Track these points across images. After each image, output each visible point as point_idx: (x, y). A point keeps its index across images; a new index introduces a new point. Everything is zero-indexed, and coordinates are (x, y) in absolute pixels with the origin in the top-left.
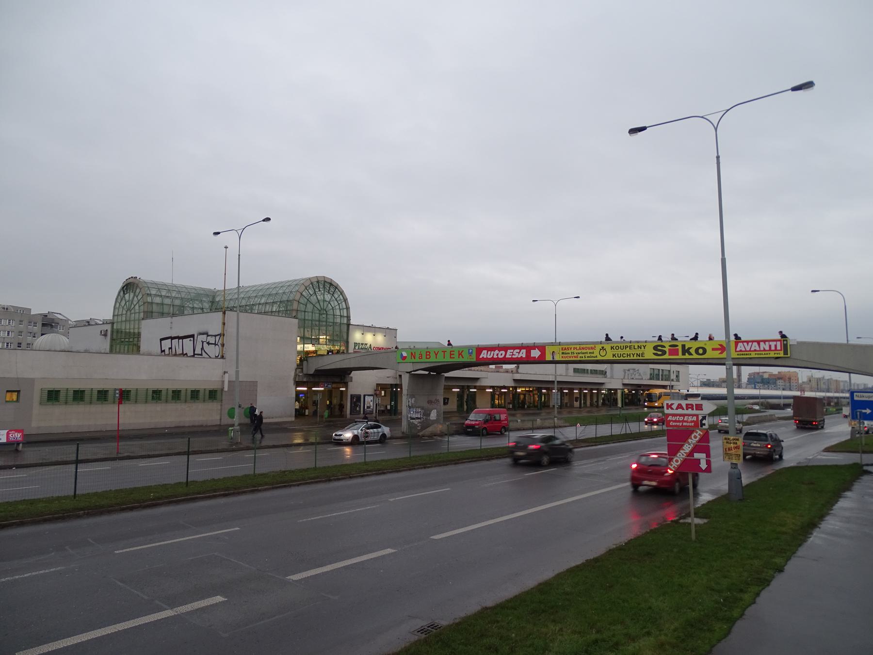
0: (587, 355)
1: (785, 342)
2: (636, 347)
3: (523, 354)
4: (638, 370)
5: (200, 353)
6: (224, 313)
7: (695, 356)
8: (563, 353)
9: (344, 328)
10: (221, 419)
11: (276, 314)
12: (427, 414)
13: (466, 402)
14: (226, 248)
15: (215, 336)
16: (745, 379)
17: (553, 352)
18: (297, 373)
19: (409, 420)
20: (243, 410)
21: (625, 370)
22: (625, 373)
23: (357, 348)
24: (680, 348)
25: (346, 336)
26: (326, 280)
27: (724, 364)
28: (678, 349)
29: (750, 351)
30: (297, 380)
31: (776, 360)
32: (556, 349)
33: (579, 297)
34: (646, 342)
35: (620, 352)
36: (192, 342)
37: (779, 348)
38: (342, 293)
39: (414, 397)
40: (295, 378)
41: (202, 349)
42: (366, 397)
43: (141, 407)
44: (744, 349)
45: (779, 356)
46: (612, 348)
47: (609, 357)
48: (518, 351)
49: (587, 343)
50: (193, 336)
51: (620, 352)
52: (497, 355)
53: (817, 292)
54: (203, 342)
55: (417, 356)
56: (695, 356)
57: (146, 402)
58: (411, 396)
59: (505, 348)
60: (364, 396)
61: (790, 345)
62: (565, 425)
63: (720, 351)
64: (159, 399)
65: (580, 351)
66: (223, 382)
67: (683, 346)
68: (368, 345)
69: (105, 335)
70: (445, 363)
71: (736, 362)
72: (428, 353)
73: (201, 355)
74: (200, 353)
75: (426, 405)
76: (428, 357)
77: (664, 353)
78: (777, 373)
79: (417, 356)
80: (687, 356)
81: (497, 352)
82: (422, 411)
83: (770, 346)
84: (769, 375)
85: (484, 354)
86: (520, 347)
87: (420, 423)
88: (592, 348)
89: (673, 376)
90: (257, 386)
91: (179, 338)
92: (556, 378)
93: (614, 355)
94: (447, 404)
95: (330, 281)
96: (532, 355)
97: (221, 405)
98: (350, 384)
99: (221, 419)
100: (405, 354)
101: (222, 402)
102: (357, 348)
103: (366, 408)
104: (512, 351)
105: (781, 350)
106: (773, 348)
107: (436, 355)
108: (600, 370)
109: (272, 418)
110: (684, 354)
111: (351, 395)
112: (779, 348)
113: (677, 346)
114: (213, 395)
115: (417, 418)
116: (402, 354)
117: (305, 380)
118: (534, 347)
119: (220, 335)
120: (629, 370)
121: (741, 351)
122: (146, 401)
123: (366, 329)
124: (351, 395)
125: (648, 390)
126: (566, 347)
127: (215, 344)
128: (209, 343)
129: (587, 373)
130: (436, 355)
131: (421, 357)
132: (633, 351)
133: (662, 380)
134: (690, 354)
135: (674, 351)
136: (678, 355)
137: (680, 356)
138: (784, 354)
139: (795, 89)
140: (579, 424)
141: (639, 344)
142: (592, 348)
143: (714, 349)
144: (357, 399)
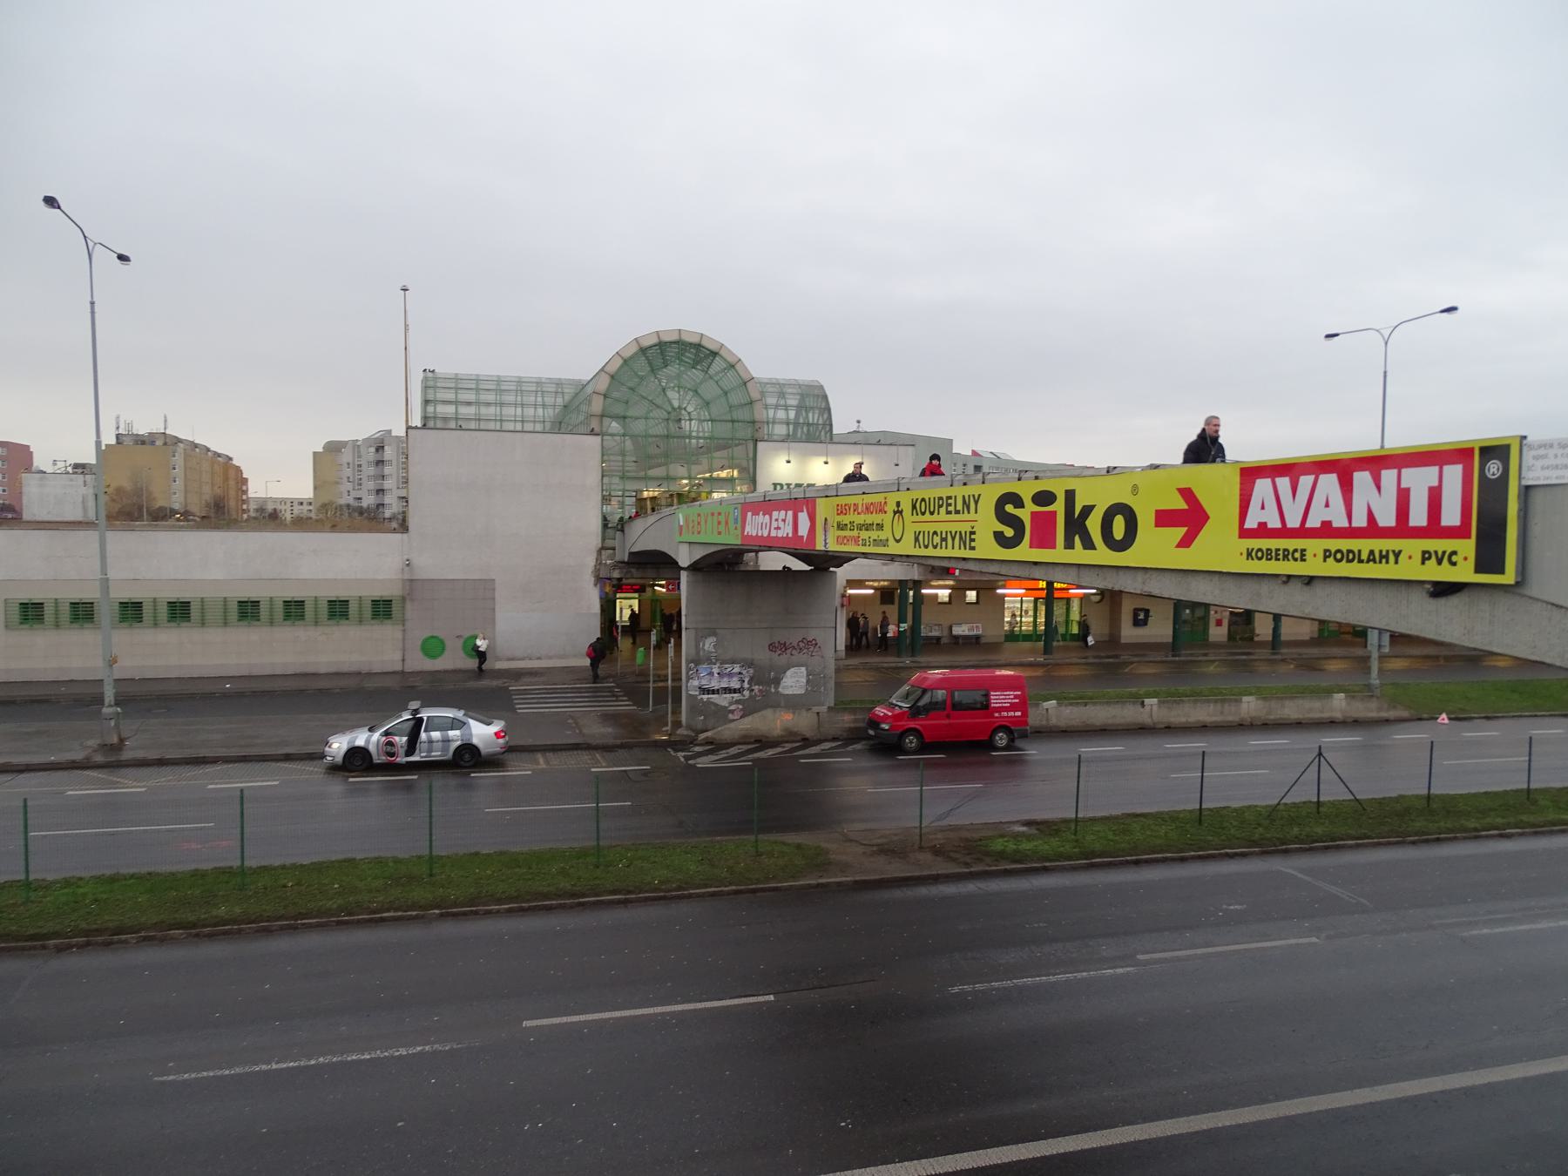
1: (1494, 468)
8: (841, 527)
10: (403, 660)
14: (859, 422)
18: (603, 557)
19: (694, 697)
20: (462, 640)
21: (1303, 560)
28: (1054, 513)
29: (1303, 532)
31: (1442, 601)
37: (1451, 516)
39: (715, 634)
43: (214, 635)
44: (1275, 523)
45: (1446, 574)
57: (226, 624)
61: (1527, 491)
62: (1384, 715)
63: (1180, 532)
64: (302, 617)
70: (729, 547)
82: (748, 673)
83: (1403, 497)
94: (1146, 624)
97: (404, 631)
99: (403, 660)
101: (404, 625)
105: (1460, 532)
106: (1418, 517)
109: (539, 658)
112: (1451, 516)
114: (382, 609)
115: (725, 689)
121: (1263, 531)
122: (156, 624)
138: (1480, 568)
140: (1444, 716)
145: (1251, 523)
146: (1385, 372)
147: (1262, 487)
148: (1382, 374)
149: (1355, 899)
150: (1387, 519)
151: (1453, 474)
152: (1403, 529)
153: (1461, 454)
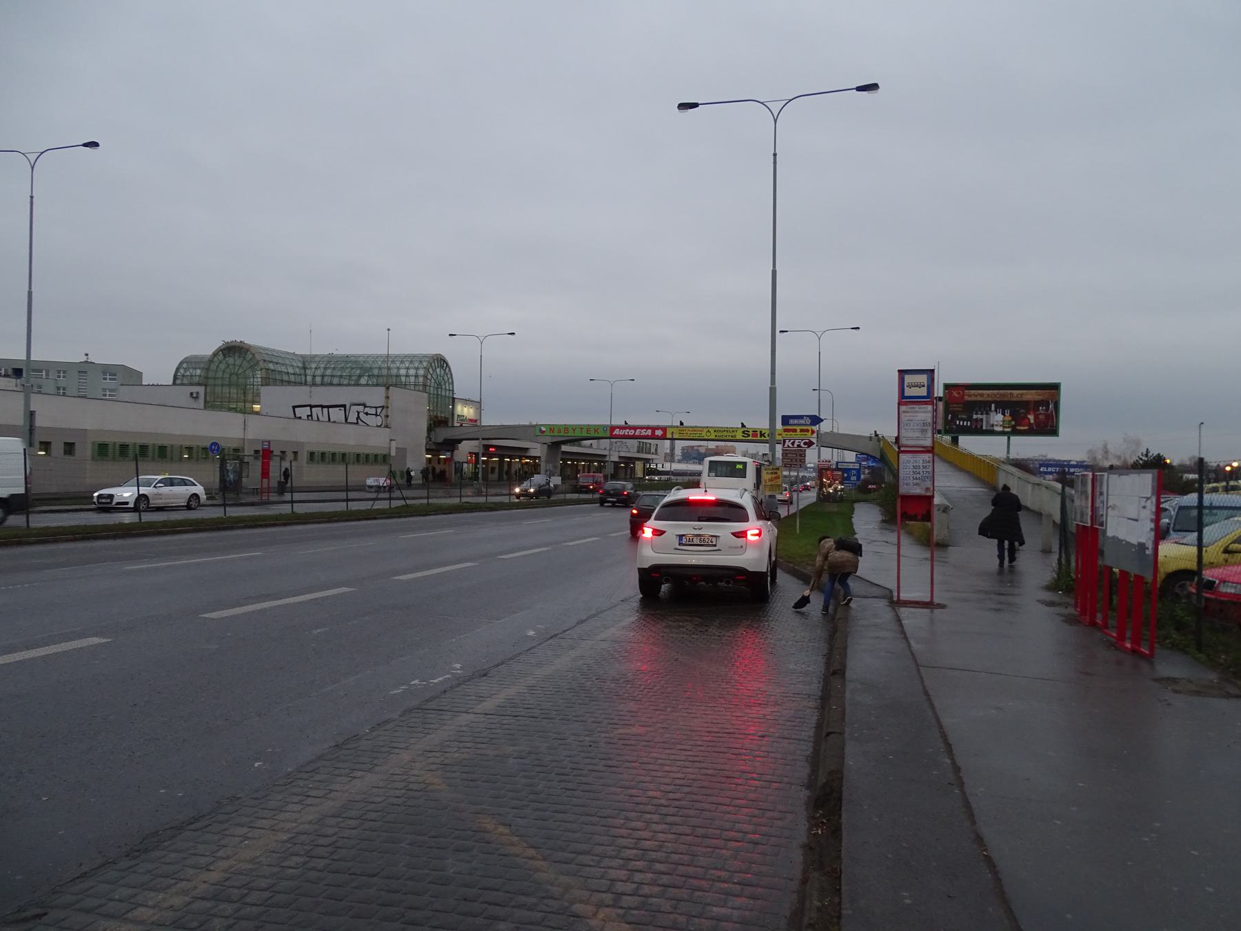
3: (649, 432)
6: (388, 388)
9: (451, 400)
11: (403, 386)
13: (429, 472)
14: (389, 330)
15: (376, 408)
16: (678, 452)
17: (672, 433)
24: (759, 433)
32: (672, 430)
33: (514, 334)
35: (720, 434)
40: (426, 446)
41: (358, 418)
46: (715, 431)
47: (713, 437)
50: (344, 406)
51: (720, 434)
54: (358, 413)
58: (547, 462)
59: (635, 428)
67: (761, 432)
69: (197, 398)
73: (357, 423)
74: (356, 422)
77: (749, 435)
78: (714, 447)
80: (763, 438)
81: (628, 430)
84: (706, 449)
85: (617, 432)
86: (647, 428)
88: (701, 431)
89: (653, 450)
90: (406, 452)
91: (322, 407)
93: (716, 436)
96: (656, 434)
100: (543, 429)
110: (761, 437)
113: (757, 431)
118: (658, 428)
119: (383, 407)
123: (467, 402)
127: (376, 415)
128: (367, 414)
131: (559, 431)
132: (730, 434)
133: (646, 453)
134: (765, 437)
136: (757, 437)
137: (759, 438)
139: (860, 89)
142: (701, 431)
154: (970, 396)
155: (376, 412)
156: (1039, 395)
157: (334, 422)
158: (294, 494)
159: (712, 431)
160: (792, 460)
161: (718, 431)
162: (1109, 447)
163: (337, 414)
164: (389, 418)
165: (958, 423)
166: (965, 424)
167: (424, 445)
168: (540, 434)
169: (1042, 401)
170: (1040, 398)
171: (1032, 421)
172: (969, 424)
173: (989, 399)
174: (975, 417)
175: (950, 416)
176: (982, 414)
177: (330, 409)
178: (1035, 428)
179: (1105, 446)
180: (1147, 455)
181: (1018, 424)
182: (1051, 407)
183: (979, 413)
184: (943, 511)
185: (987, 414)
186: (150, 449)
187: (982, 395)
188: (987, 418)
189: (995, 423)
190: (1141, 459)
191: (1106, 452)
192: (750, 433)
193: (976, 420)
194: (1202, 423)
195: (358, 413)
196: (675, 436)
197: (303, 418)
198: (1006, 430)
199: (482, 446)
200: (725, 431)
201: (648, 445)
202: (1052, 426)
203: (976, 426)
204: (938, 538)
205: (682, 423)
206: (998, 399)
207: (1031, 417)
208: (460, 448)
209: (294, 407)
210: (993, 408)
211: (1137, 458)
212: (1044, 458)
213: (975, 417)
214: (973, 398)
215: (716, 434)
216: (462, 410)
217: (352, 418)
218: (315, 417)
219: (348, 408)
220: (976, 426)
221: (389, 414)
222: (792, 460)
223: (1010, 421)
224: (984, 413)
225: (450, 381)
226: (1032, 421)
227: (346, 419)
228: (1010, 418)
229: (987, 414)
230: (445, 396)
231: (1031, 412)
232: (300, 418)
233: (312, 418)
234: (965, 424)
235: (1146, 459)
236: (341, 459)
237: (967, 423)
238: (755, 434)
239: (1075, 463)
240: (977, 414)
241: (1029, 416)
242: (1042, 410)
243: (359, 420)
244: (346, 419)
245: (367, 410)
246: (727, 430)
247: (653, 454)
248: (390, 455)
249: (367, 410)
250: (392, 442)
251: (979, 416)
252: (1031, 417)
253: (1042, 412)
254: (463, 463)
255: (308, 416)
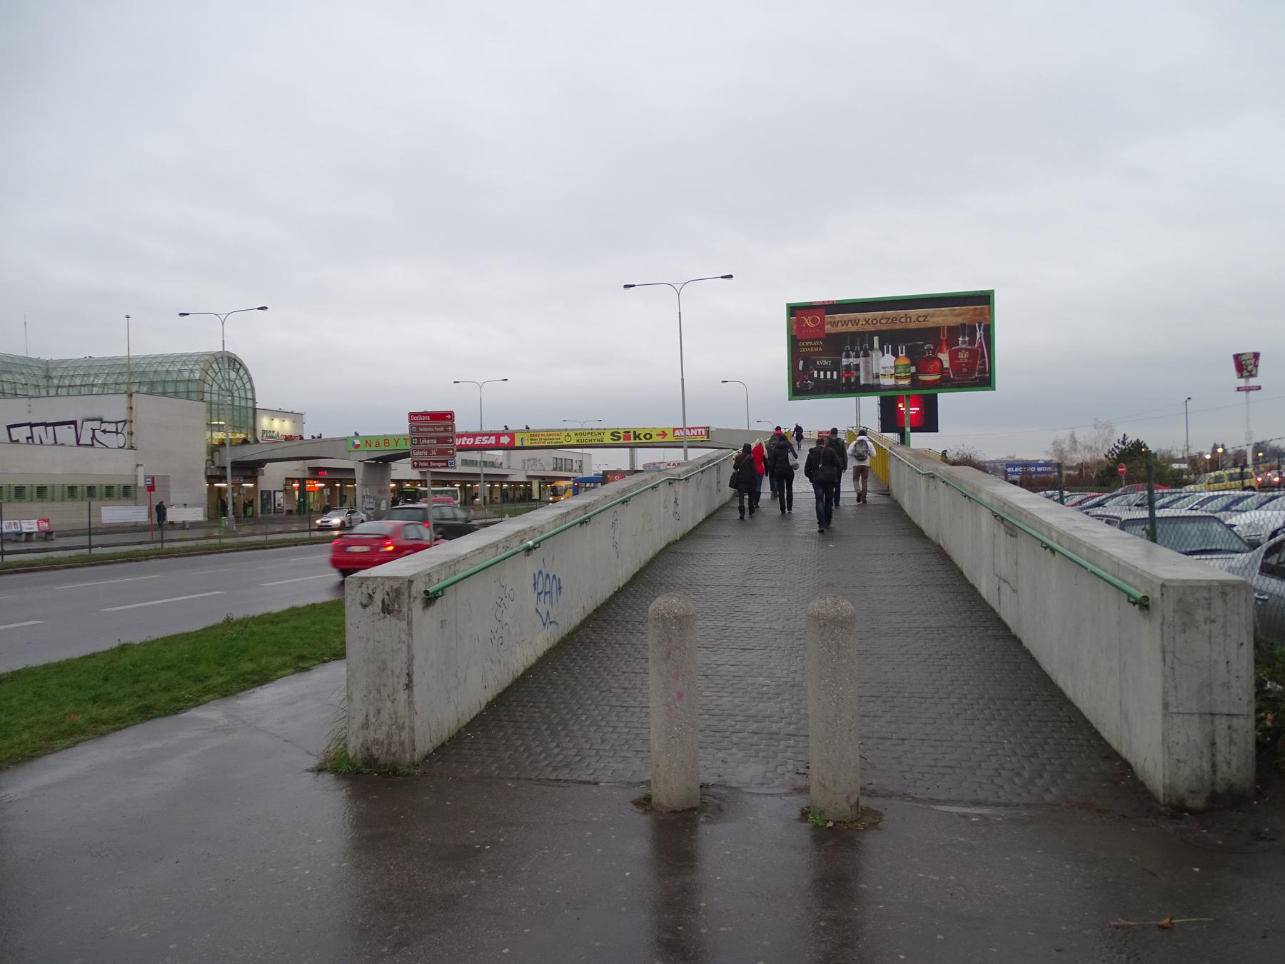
0: (553, 441)
2: (597, 433)
3: (493, 440)
4: (540, 460)
5: (80, 443)
6: (131, 396)
7: (644, 440)
8: (531, 440)
9: (250, 412)
12: (378, 505)
14: (128, 317)
15: (116, 423)
17: (522, 439)
21: (524, 460)
22: (525, 463)
23: (265, 436)
24: (632, 434)
25: (252, 422)
26: (231, 356)
27: (682, 447)
30: (209, 474)
32: (525, 436)
34: (605, 429)
35: (582, 438)
36: (73, 430)
37: (703, 433)
38: (246, 371)
40: (206, 472)
41: (93, 437)
42: (277, 493)
46: (576, 434)
47: (574, 442)
48: (488, 437)
49: (554, 430)
50: (74, 423)
51: (582, 438)
52: (466, 442)
53: (631, 288)
54: (94, 430)
55: (373, 444)
56: (644, 440)
57: (63, 500)
58: (365, 485)
59: (474, 436)
60: (275, 492)
65: (547, 437)
66: (136, 476)
67: (635, 432)
68: (276, 433)
71: (691, 444)
72: (387, 441)
73: (92, 445)
75: (376, 494)
76: (387, 444)
77: (619, 438)
79: (373, 444)
80: (638, 441)
81: (465, 439)
83: (698, 432)
86: (490, 435)
87: (373, 513)
89: (576, 467)
90: (169, 481)
91: (46, 425)
92: (482, 470)
93: (578, 441)
95: (234, 357)
96: (501, 442)
98: (260, 477)
102: (265, 436)
103: (276, 505)
104: (481, 438)
106: (700, 434)
107: (397, 442)
108: (490, 462)
110: (635, 439)
111: (262, 492)
112: (703, 433)
113: (629, 432)
116: (354, 443)
117: (218, 474)
119: (125, 421)
120: (529, 460)
121: (677, 436)
123: (275, 413)
124: (262, 492)
125: (551, 483)
126: (535, 434)
127: (117, 432)
128: (104, 431)
129: (476, 465)
130: (397, 442)
131: (378, 444)
132: (594, 437)
133: (565, 471)
134: (640, 439)
135: (627, 437)
136: (630, 440)
137: (632, 441)
141: (599, 431)
143: (658, 435)
144: (268, 496)
145: (676, 435)
146: (223, 341)
147: (677, 431)
148: (222, 343)
149: (567, 479)
150: (696, 434)
151: (703, 430)
152: (698, 435)
153: (704, 428)
154: (834, 324)
155: (117, 429)
156: (958, 315)
157: (63, 444)
158: (92, 537)
159: (572, 434)
160: (429, 451)
161: (581, 434)
162: (1077, 436)
163: (66, 434)
164: (133, 436)
165: (815, 376)
166: (829, 377)
167: (203, 471)
168: (352, 449)
169: (963, 325)
170: (959, 320)
171: (946, 365)
172: (835, 377)
173: (870, 328)
174: (845, 362)
175: (801, 362)
176: (857, 356)
177: (57, 428)
178: (952, 377)
179: (1073, 436)
180: (1124, 443)
181: (919, 372)
182: (978, 336)
183: (852, 354)
184: (386, 609)
185: (866, 355)
186: (79, 489)
187: (855, 322)
188: (867, 363)
189: (882, 372)
190: (1117, 447)
191: (1074, 441)
192: (621, 435)
193: (848, 366)
194: (1189, 398)
195: (94, 430)
196: (526, 444)
197: (21, 441)
198: (901, 382)
199: (307, 469)
200: (588, 434)
201: (569, 462)
202: (982, 371)
203: (848, 379)
204: (371, 735)
205: (528, 428)
206: (884, 328)
207: (944, 357)
208: (265, 472)
209: (9, 427)
210: (876, 345)
211: (1113, 446)
212: (1012, 459)
213: (845, 362)
214: (840, 329)
215: (579, 438)
216: (271, 424)
217: (86, 439)
218: (37, 440)
219: (79, 424)
220: (848, 379)
221: (133, 430)
222: (429, 451)
223: (907, 366)
224: (862, 353)
225: (248, 386)
226: (946, 365)
227: (78, 441)
228: (907, 362)
229: (866, 355)
230: (247, 407)
231: (944, 348)
232: (17, 441)
233: (33, 441)
234: (829, 377)
235: (1124, 447)
236: (122, 494)
237: (832, 375)
238: (627, 437)
239: (1043, 462)
240: (848, 356)
241: (941, 356)
242: (964, 342)
243: (95, 441)
244: (78, 441)
245: (105, 426)
246: (591, 432)
247: (575, 471)
248: (136, 485)
249: (105, 426)
250: (139, 467)
251: (853, 361)
252: (944, 357)
253: (964, 346)
254: (275, 492)
255: (28, 438)
